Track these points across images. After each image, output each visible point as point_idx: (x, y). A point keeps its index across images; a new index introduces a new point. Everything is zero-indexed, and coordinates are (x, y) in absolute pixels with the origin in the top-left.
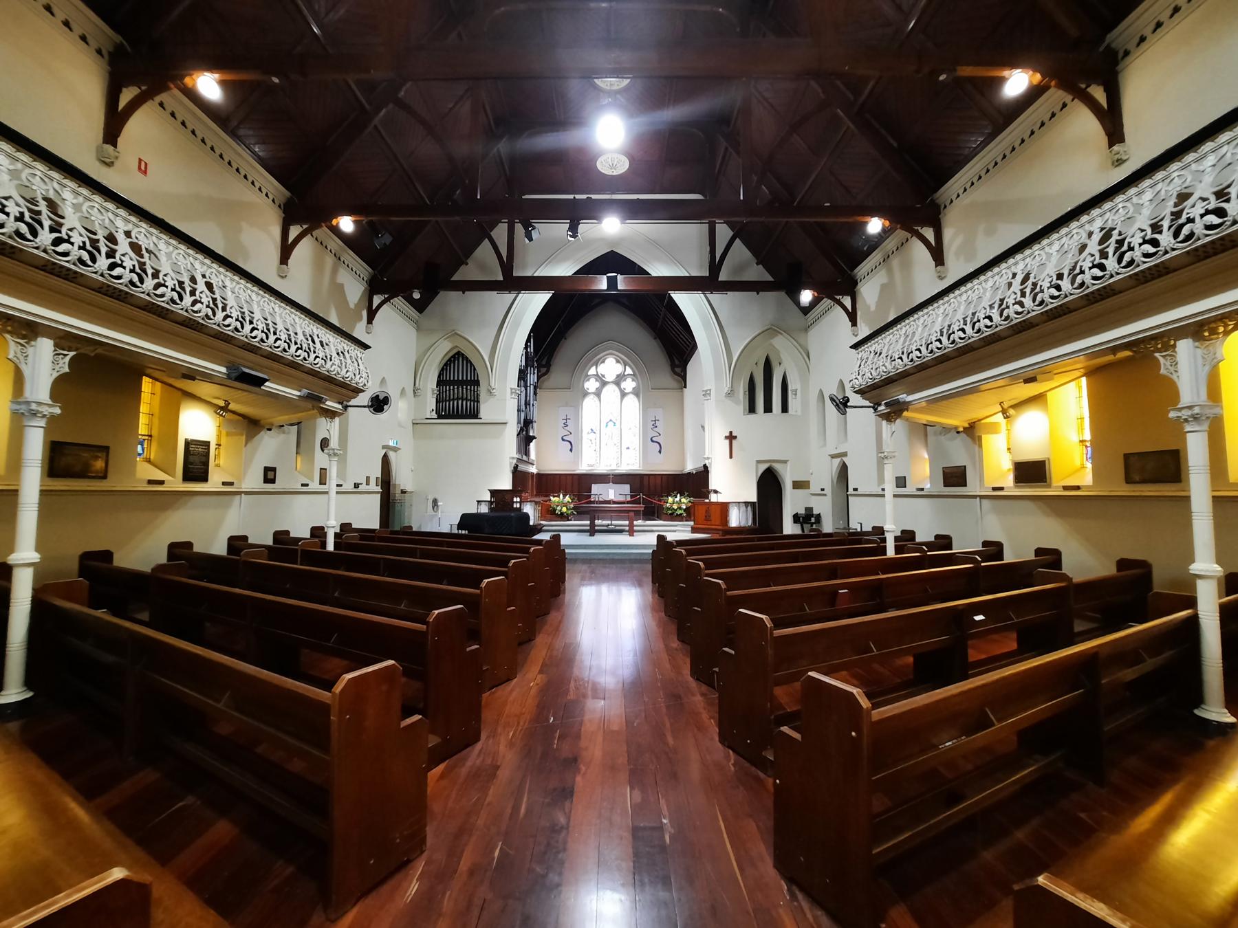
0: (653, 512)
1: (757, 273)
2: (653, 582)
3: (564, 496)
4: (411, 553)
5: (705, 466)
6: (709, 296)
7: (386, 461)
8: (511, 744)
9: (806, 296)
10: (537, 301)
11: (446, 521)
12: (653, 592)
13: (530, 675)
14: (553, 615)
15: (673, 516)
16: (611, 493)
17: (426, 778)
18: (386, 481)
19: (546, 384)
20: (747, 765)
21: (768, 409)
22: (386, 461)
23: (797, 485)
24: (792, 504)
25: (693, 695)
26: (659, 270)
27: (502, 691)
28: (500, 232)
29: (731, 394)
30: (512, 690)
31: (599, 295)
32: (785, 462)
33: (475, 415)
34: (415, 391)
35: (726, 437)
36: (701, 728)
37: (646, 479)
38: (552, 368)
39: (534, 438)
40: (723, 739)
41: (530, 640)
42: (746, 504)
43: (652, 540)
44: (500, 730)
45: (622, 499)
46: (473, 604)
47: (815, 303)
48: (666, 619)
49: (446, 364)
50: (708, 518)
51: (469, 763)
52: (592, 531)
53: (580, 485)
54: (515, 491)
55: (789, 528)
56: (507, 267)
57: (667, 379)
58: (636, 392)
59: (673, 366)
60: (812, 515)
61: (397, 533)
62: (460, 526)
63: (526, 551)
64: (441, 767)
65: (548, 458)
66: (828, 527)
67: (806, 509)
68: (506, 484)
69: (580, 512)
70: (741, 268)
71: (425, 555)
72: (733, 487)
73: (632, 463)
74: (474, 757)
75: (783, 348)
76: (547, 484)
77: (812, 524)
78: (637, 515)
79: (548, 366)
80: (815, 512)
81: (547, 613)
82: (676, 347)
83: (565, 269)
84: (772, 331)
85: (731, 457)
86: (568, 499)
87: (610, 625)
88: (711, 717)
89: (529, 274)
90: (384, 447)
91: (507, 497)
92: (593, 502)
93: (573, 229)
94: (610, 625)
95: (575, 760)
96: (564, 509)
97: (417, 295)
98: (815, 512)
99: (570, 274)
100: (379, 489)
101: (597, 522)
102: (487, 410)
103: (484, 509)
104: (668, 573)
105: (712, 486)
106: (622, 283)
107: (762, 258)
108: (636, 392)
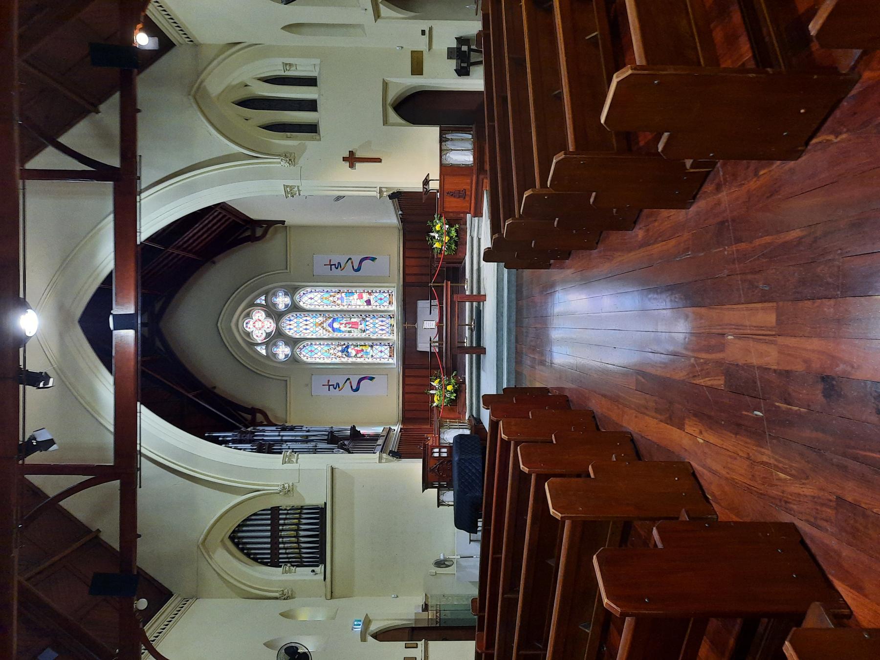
0: (454, 271)
1: (109, 114)
2: (548, 266)
3: (433, 388)
4: (510, 605)
5: (392, 196)
6: (144, 183)
7: (383, 635)
8: (801, 476)
9: (142, 40)
10: (154, 431)
11: (465, 548)
12: (562, 267)
13: (686, 442)
14: (597, 405)
15: (459, 242)
16: (428, 325)
17: (726, 525)
18: (411, 633)
19: (280, 414)
20: (838, 113)
21: (311, 105)
22: (383, 635)
23: (417, 68)
24: (443, 77)
25: (719, 203)
26: (105, 258)
27: (711, 485)
28: (50, 485)
29: (290, 158)
30: (710, 470)
31: (145, 343)
32: (385, 85)
33: (320, 511)
34: (286, 596)
35: (352, 166)
36: (772, 191)
37: (410, 279)
38: (258, 405)
39: (353, 428)
40: (793, 154)
41: (632, 440)
42: (442, 140)
43: (490, 270)
44: (774, 492)
45: (436, 311)
46: (588, 536)
47: (152, 29)
48: (601, 247)
49: (248, 555)
50: (461, 194)
51: (833, 543)
52: (479, 350)
53: (417, 367)
54: (425, 455)
55: (475, 82)
56: (98, 474)
57: (270, 249)
58: (292, 291)
59: (253, 239)
60: (459, 49)
61: (481, 619)
62: (472, 529)
63: (506, 445)
64: (841, 587)
65: (381, 408)
66: (473, 27)
67: (450, 57)
68: (415, 467)
69: (454, 368)
70: (103, 135)
71: (512, 586)
72: (419, 159)
73: (387, 300)
74: (823, 537)
75: (220, 81)
76: (417, 414)
77: (470, 50)
78: (457, 290)
79: (253, 411)
80: (454, 45)
81: (593, 416)
82: (221, 234)
83: (105, 387)
84: (198, 96)
85: (378, 160)
86: (435, 383)
87: (603, 327)
88: (756, 174)
89: (110, 439)
90: (363, 639)
91: (432, 464)
92: (440, 348)
93: (37, 379)
94: (603, 327)
95: (825, 379)
96: (450, 388)
97: (142, 604)
98: (454, 45)
99: (110, 379)
100: (421, 644)
101: (467, 344)
102: (315, 496)
103: (449, 496)
104: (538, 246)
105: (418, 187)
106: (125, 307)
107: (88, 106)
108: (292, 291)
